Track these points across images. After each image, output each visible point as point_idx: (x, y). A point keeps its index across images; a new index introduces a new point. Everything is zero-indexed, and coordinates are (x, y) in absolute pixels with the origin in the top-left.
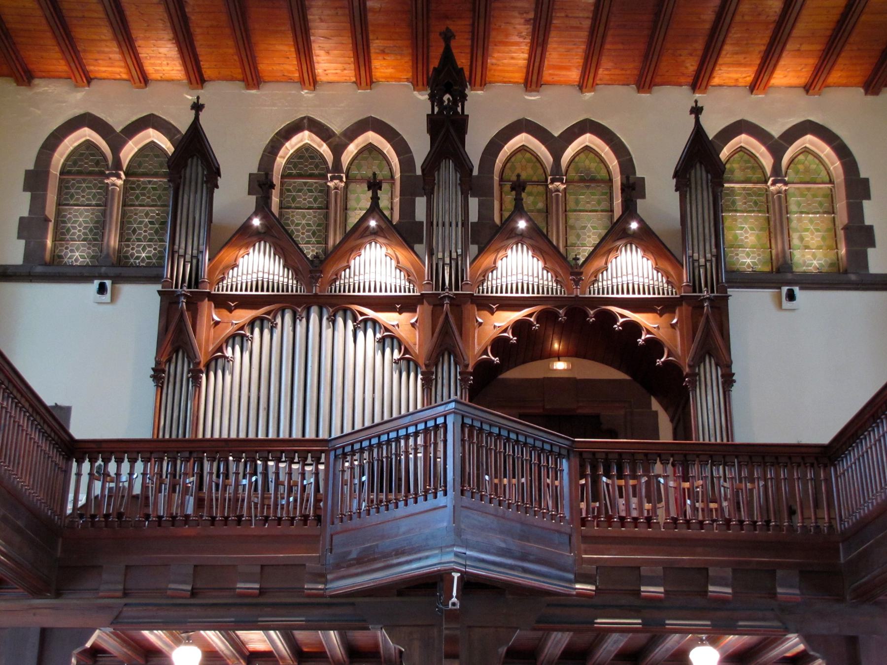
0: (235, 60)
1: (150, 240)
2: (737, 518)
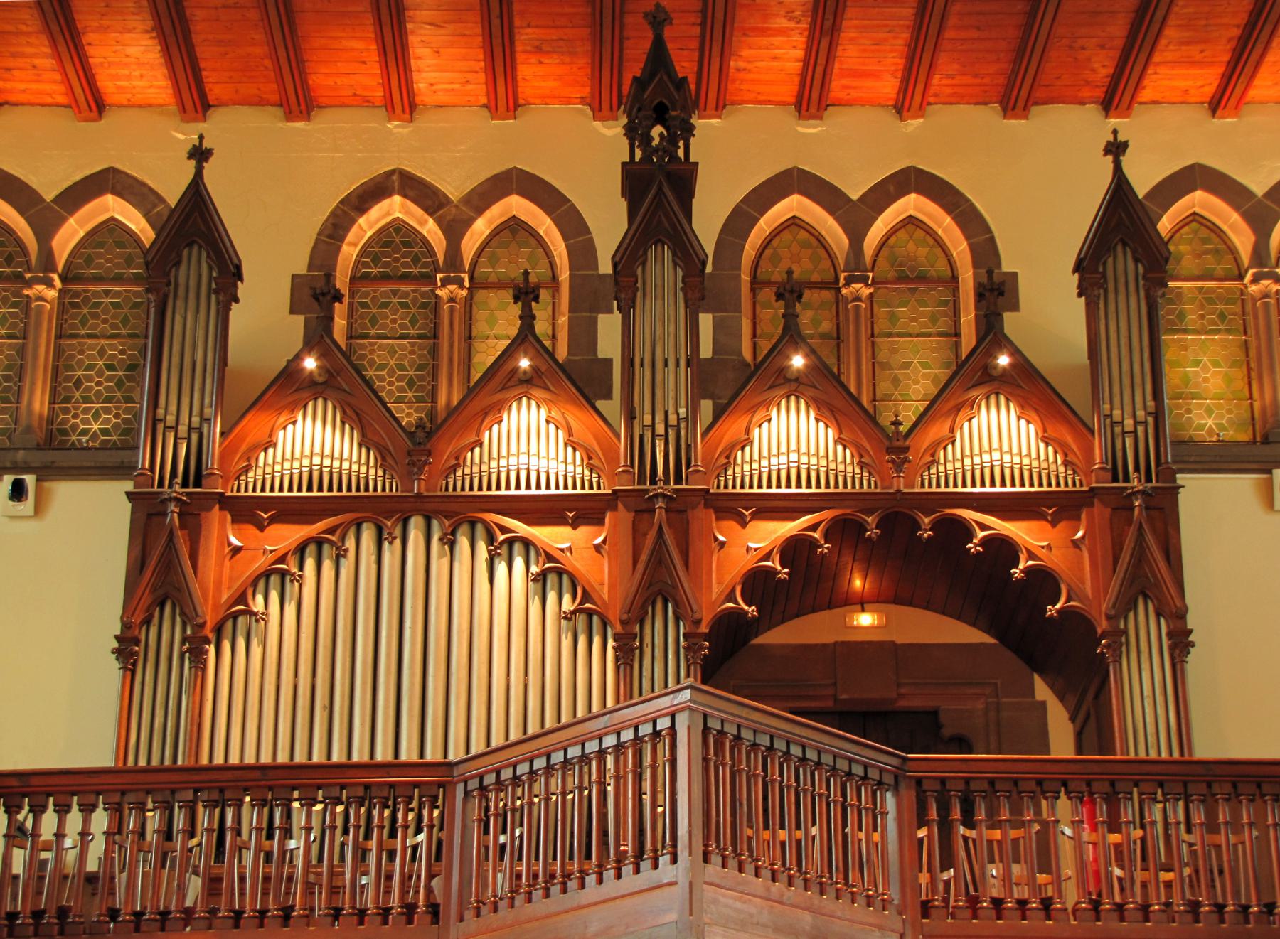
0: (266, 68)
1: (108, 400)
2: (1163, 899)
